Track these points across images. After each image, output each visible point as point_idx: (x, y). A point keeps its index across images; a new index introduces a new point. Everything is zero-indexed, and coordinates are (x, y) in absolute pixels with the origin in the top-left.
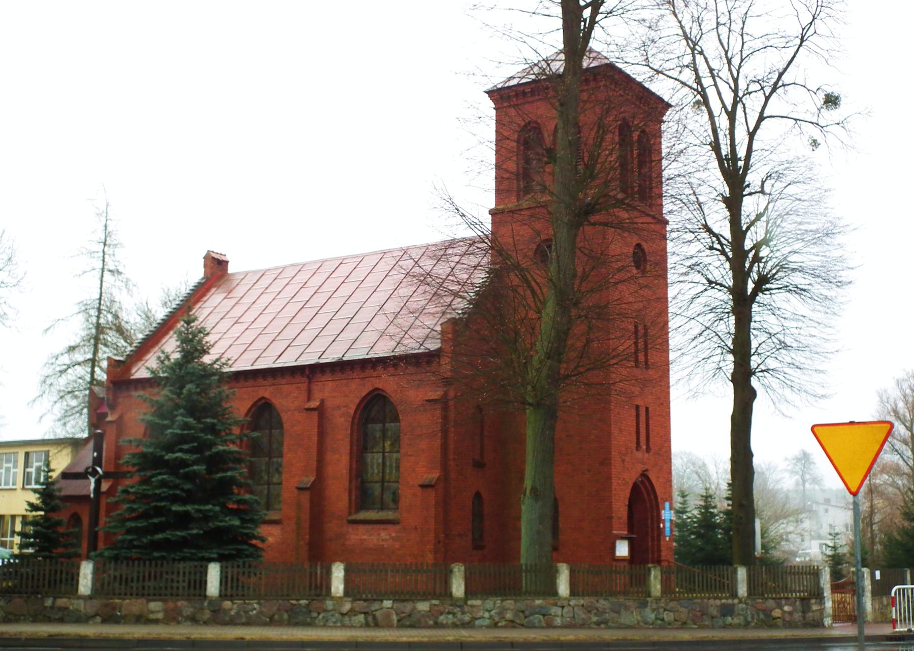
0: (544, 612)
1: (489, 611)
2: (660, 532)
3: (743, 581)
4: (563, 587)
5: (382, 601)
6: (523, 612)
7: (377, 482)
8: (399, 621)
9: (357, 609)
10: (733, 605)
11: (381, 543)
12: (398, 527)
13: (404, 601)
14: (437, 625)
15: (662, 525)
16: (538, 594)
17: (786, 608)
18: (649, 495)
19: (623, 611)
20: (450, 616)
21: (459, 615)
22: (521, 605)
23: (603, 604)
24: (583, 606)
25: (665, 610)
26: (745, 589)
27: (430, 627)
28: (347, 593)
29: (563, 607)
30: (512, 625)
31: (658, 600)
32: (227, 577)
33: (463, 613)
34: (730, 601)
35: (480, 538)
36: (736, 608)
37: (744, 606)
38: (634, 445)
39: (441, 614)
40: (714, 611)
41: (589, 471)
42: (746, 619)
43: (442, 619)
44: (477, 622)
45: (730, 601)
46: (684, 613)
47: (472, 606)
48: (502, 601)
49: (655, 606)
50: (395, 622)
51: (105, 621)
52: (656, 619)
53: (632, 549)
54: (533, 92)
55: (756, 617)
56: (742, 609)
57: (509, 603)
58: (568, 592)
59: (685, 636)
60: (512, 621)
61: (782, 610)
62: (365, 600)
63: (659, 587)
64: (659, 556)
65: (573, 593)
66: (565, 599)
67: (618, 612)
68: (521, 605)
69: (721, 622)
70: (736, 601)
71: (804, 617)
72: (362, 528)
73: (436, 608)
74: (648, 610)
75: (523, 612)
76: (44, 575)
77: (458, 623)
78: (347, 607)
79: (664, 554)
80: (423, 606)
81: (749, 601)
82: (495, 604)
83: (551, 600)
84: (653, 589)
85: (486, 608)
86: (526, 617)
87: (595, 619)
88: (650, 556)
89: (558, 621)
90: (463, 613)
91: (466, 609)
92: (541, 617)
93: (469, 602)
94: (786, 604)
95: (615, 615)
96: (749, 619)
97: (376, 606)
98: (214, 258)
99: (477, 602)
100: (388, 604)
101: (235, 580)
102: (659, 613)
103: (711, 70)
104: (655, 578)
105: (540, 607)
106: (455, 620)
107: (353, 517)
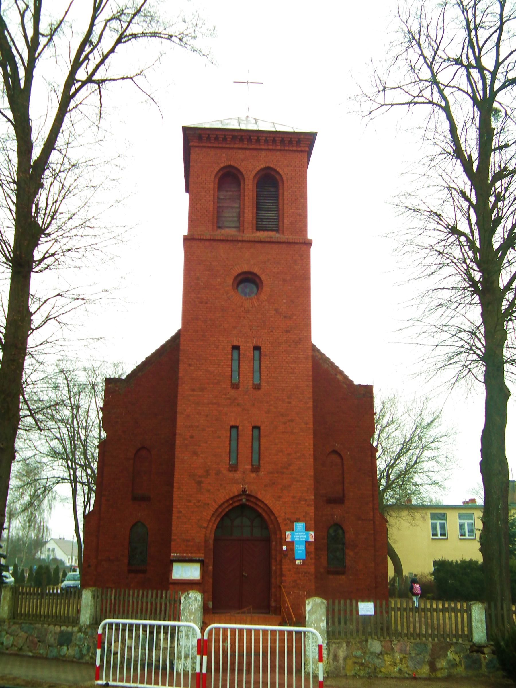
10: (72, 634)
15: (285, 548)
25: (7, 633)
32: (333, 610)
34: (70, 629)
36: (74, 638)
40: (51, 639)
45: (70, 629)
51: (177, 657)
53: (366, 599)
54: (274, 141)
56: (80, 639)
70: (76, 629)
98: (218, 188)
101: (342, 613)
103: (440, 224)
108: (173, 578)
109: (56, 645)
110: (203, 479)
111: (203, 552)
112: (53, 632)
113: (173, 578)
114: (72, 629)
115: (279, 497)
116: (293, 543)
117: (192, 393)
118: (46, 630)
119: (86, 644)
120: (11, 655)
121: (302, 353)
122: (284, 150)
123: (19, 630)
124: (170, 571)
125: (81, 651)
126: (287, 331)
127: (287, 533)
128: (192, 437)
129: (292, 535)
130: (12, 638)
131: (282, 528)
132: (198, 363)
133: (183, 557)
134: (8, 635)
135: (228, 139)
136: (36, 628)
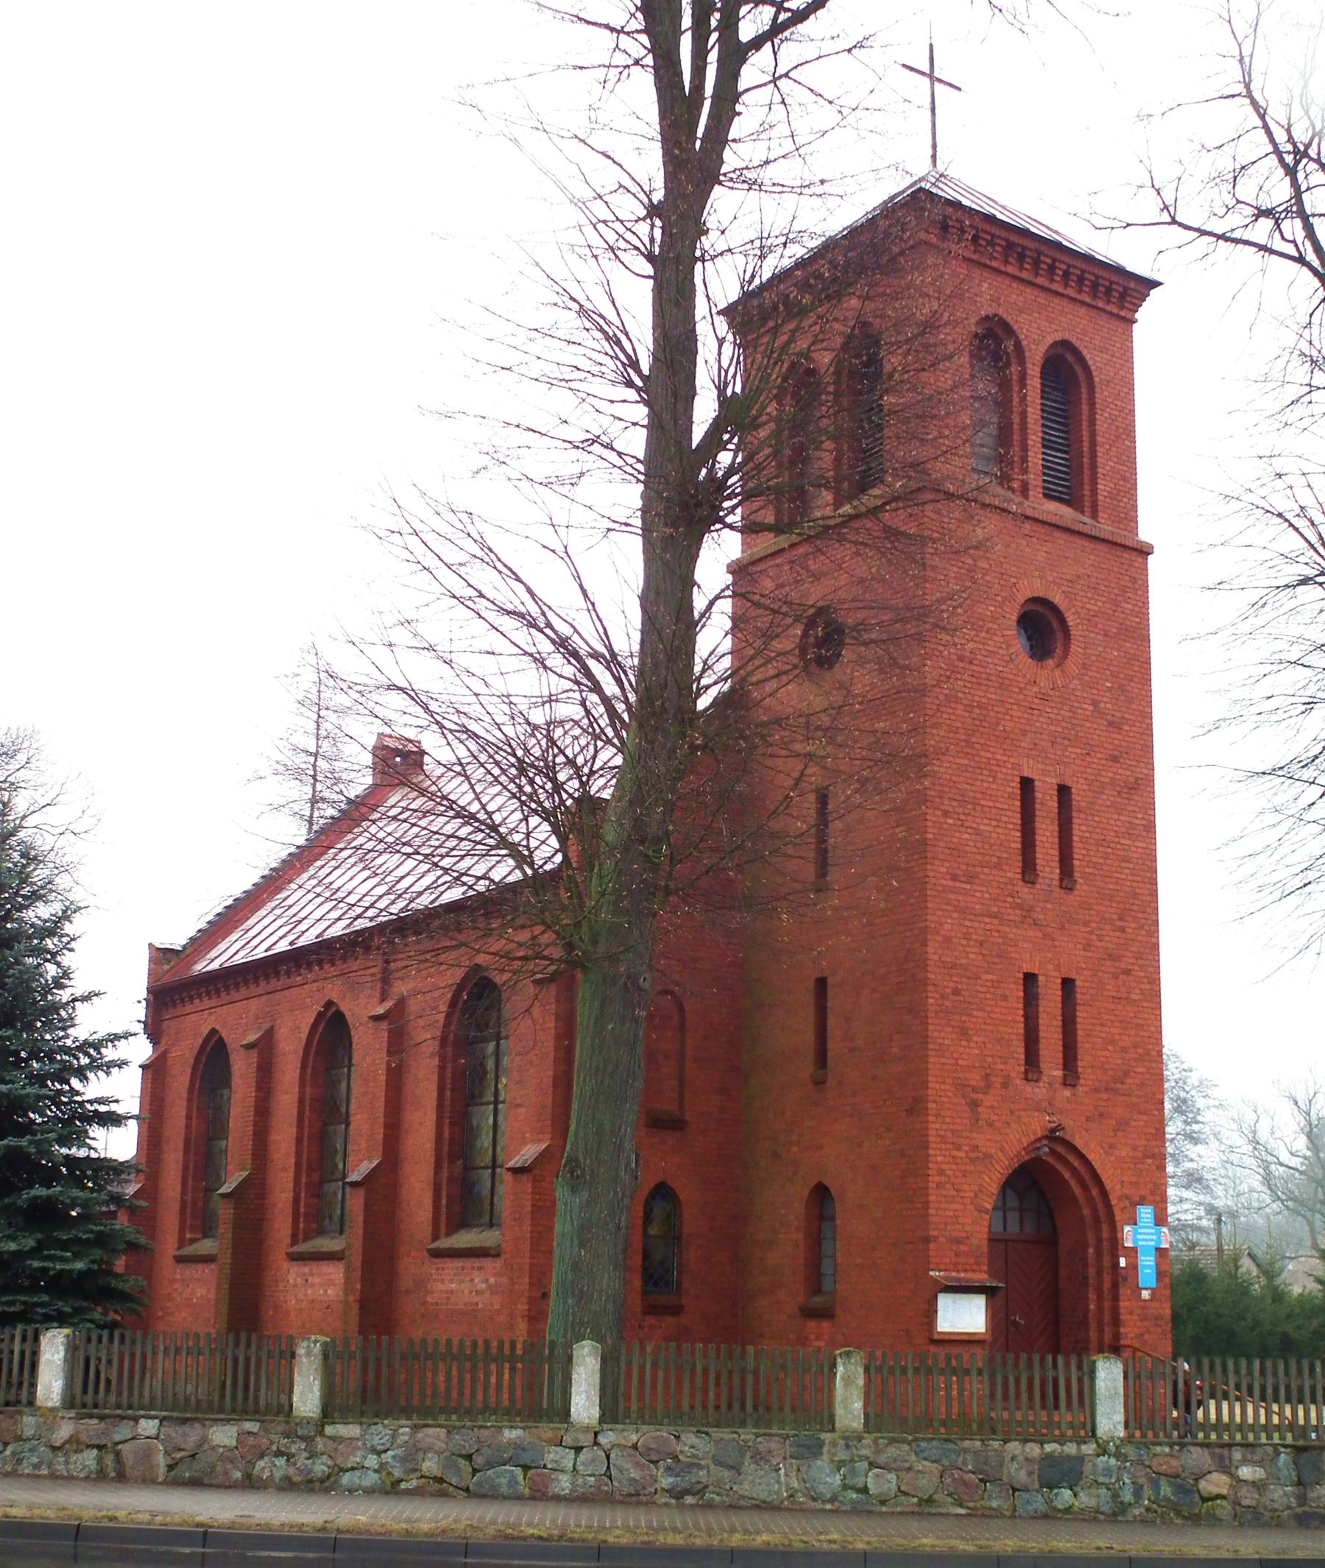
0: (526, 1458)
1: (379, 1453)
2: (1121, 1280)
3: (1112, 1397)
4: (584, 1403)
5: (136, 1419)
6: (469, 1457)
7: (486, 1168)
8: (170, 1467)
9: (84, 1438)
10: (1081, 1459)
11: (475, 1300)
12: (498, 1263)
13: (184, 1421)
14: (251, 1484)
15: (1123, 1262)
16: (512, 1414)
17: (1246, 1472)
18: (1085, 1188)
19: (748, 1466)
20: (281, 1462)
21: (302, 1460)
22: (464, 1440)
23: (692, 1443)
24: (635, 1447)
25: (872, 1465)
26: (1120, 1417)
27: (229, 1486)
28: (69, 1401)
29: (578, 1449)
30: (437, 1488)
31: (851, 1439)
33: (313, 1455)
34: (1071, 1449)
35: (711, 1293)
36: (1088, 1468)
37: (1113, 1461)
38: (1017, 1066)
39: (262, 1456)
41: (888, 1130)
42: (1115, 1496)
43: (262, 1467)
44: (346, 1479)
45: (1071, 1449)
46: (926, 1476)
47: (333, 1439)
48: (415, 1428)
49: (843, 1455)
50: (162, 1469)
52: (845, 1487)
55: (1147, 1492)
56: (1108, 1471)
57: (434, 1435)
58: (595, 1412)
59: (929, 1539)
60: (440, 1480)
61: (1232, 1476)
62: (102, 1418)
63: (858, 1405)
64: (1117, 1336)
65: (611, 1411)
66: (586, 1429)
67: (736, 1468)
68: (464, 1440)
69: (1039, 1502)
70: (1089, 1449)
71: (1302, 1499)
72: (452, 1265)
73: (251, 1441)
74: (822, 1464)
75: (469, 1457)
76: (718, 1384)
77: (297, 1479)
78: (64, 1431)
79: (1129, 1333)
80: (223, 1435)
81: (1130, 1451)
82: (394, 1437)
83: (546, 1430)
84: (839, 1411)
85: (371, 1444)
86: (475, 1471)
87: (666, 1481)
88: (1093, 1334)
89: (563, 1484)
90: (313, 1455)
91: (320, 1444)
92: (519, 1471)
93: (329, 1430)
94: (1245, 1461)
95: (726, 1474)
96: (1127, 1496)
97: (123, 1431)
99: (352, 1430)
100: (148, 1426)
102: (853, 1471)
104: (848, 1381)
105: (518, 1446)
106: (291, 1471)
107: (444, 1243)
108: (983, 1330)
109: (1037, 1486)
110: (980, 1097)
111: (985, 1268)
112: (1021, 1458)
113: (983, 1330)
114: (1079, 1448)
115: (1111, 1147)
116: (1134, 1250)
117: (951, 883)
118: (1000, 1454)
119: (1127, 1481)
120: (901, 1513)
121: (1139, 816)
122: (1093, 307)
123: (913, 1457)
124: (932, 1312)
125: (1115, 1496)
126: (1115, 759)
127: (1127, 1228)
128: (956, 992)
129: (1135, 1233)
130: (892, 1477)
131: (1117, 1218)
132: (961, 810)
133: (959, 1280)
134: (876, 1471)
135: (1072, 277)
136: (965, 1451)
